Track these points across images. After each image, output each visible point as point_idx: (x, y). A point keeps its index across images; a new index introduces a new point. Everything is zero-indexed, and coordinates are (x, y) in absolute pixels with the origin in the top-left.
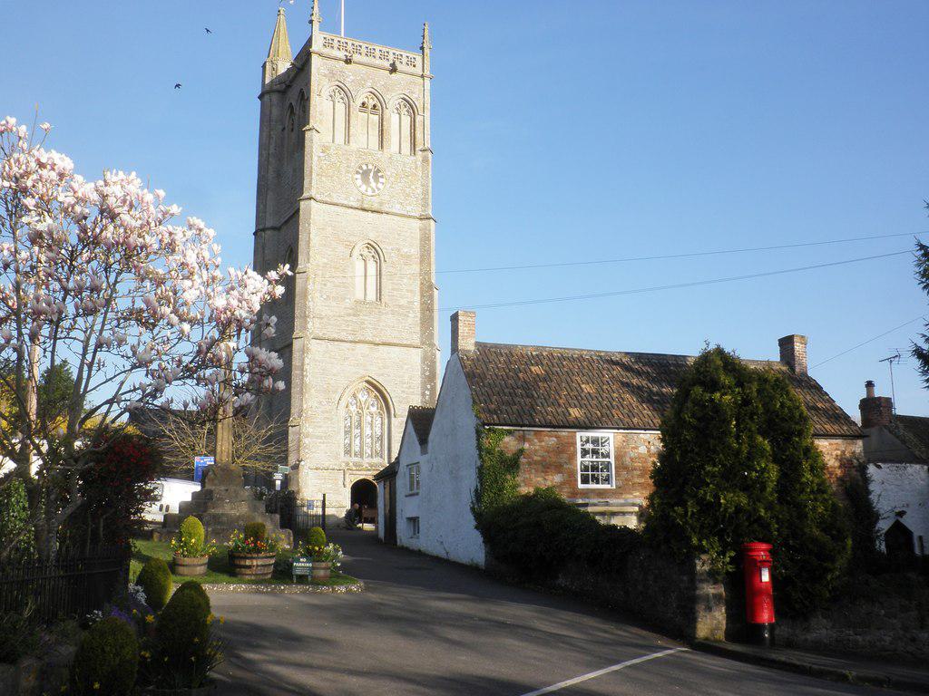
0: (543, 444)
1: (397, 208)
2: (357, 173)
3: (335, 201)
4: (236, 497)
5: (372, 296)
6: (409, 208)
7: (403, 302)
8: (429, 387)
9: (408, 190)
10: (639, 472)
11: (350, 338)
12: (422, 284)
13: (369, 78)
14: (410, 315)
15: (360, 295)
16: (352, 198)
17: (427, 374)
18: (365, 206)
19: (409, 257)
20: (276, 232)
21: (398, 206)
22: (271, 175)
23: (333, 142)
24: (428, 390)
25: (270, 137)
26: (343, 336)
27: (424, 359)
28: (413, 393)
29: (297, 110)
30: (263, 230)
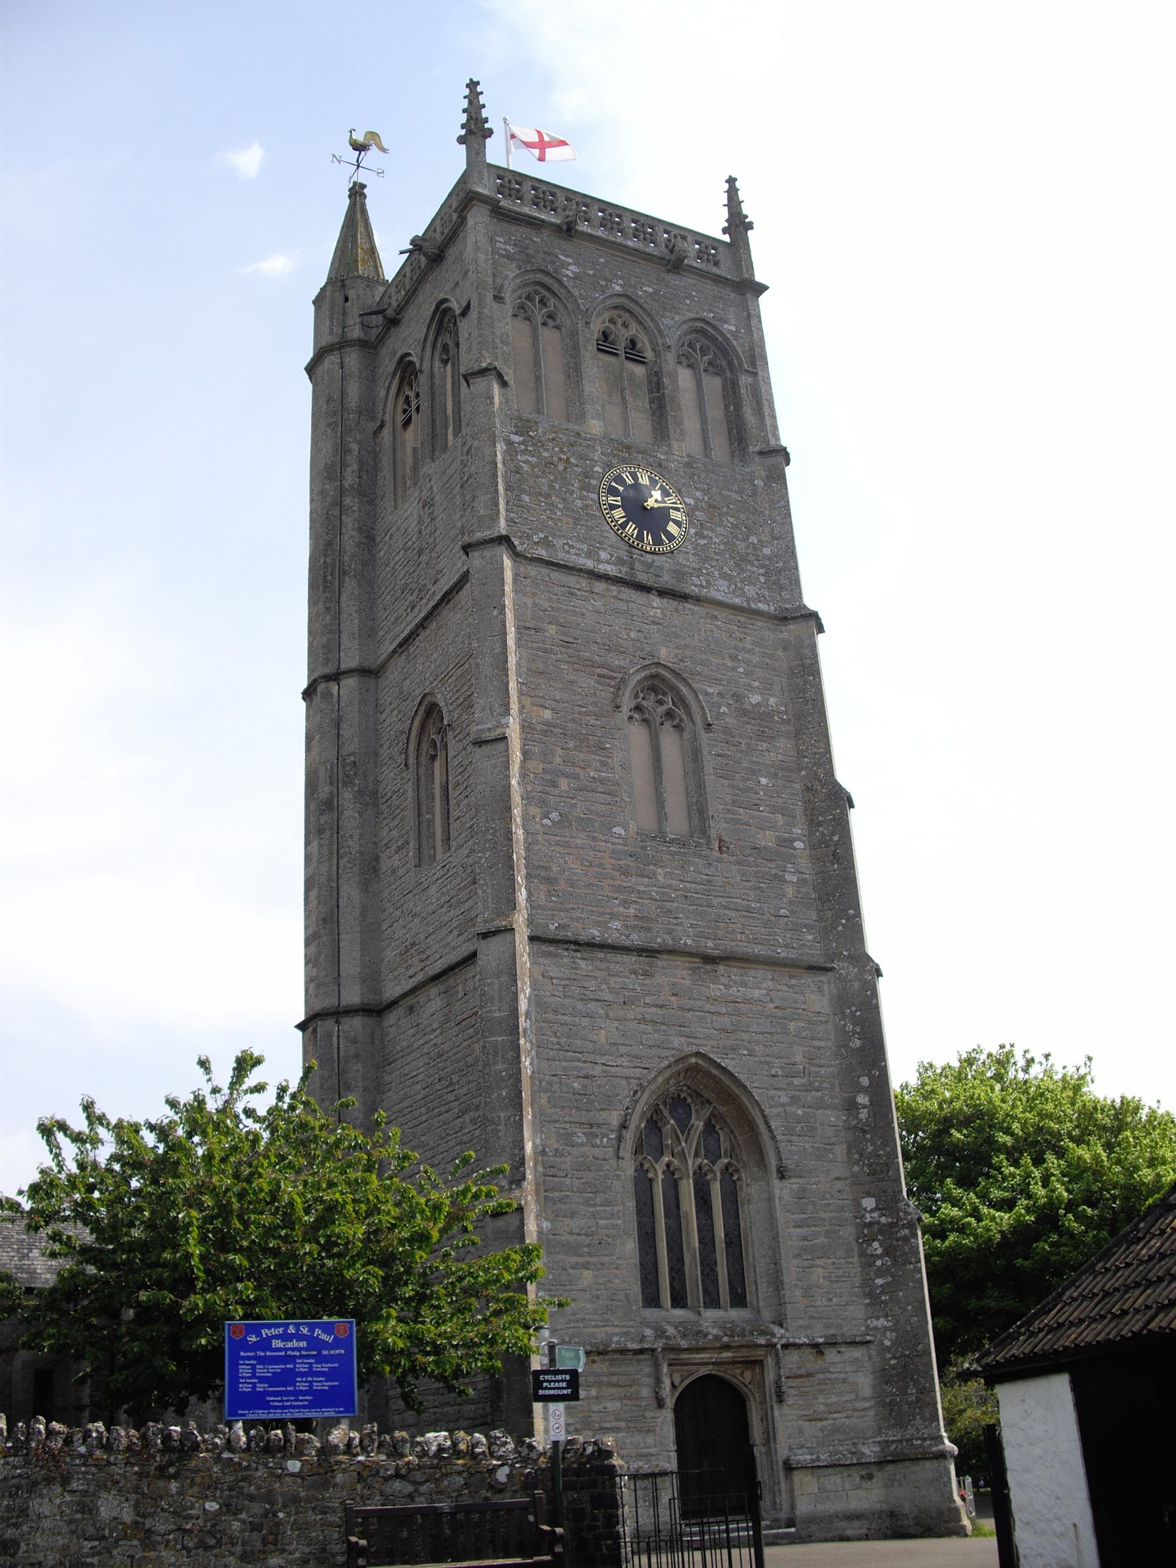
0: (1062, 1212)
1: (720, 591)
2: (613, 491)
3: (561, 557)
4: (275, 1543)
5: (678, 823)
6: (750, 590)
7: (767, 839)
8: (865, 1081)
9: (740, 546)
10: (128, 1338)
11: (636, 939)
12: (808, 789)
13: (615, 276)
14: (788, 877)
15: (645, 818)
16: (604, 555)
17: (857, 1043)
18: (642, 578)
19: (768, 716)
20: (370, 1021)
21: (723, 585)
22: (350, 538)
23: (479, 743)
24: (865, 1090)
25: (343, 450)
26: (615, 931)
27: (842, 1001)
28: (820, 1105)
29: (439, 217)
30: (336, 677)
